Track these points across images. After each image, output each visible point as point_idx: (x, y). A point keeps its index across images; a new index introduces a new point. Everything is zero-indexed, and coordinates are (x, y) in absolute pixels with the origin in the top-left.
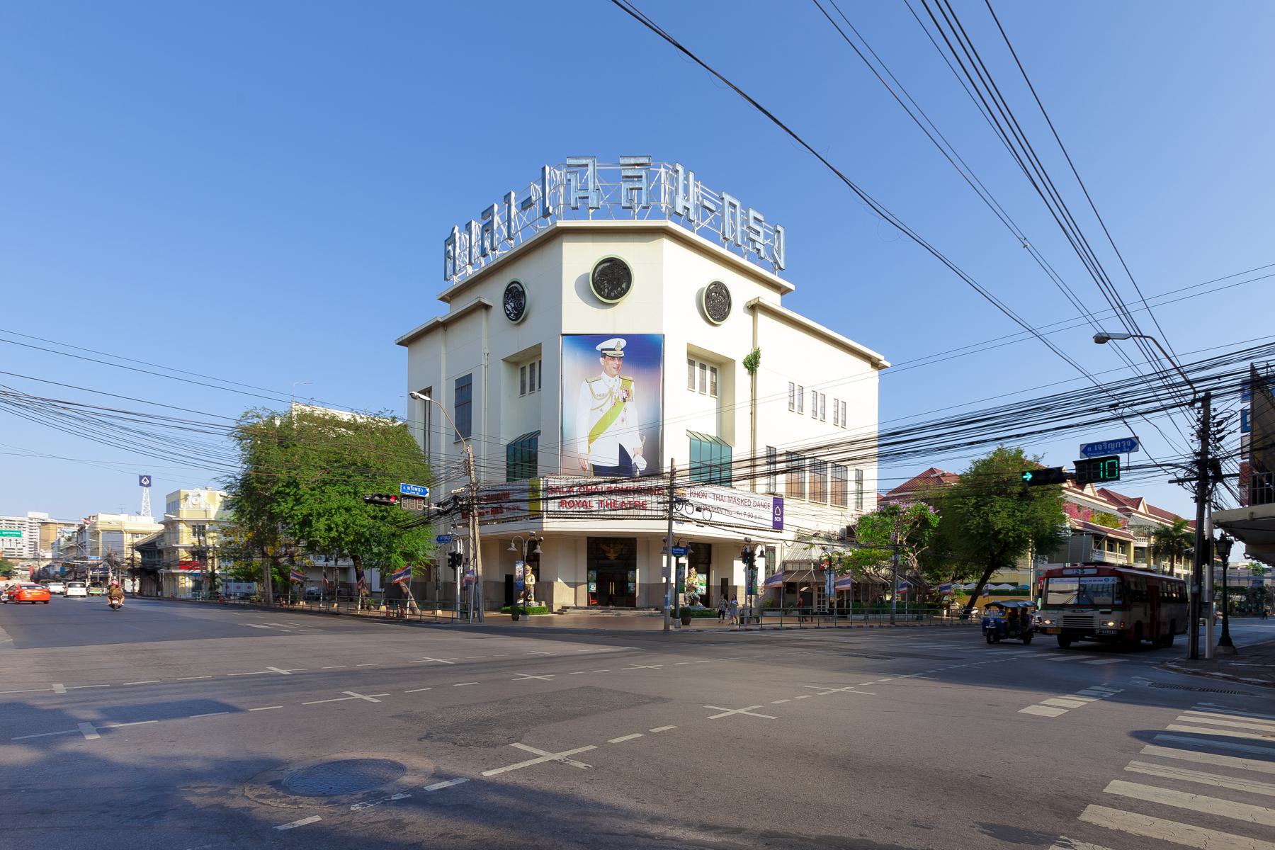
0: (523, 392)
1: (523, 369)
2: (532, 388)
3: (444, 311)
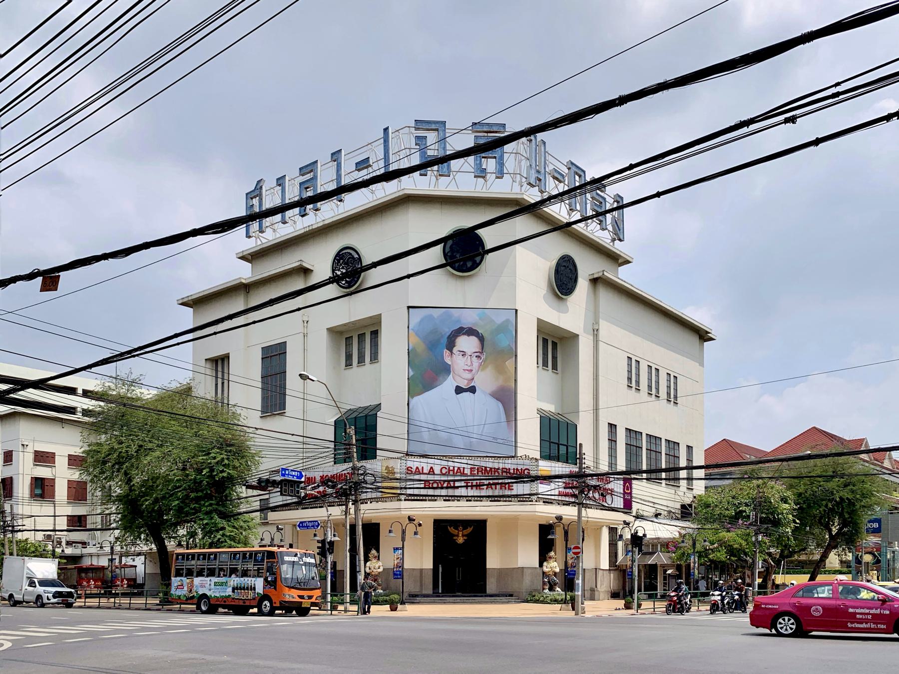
0: (349, 364)
1: (349, 340)
2: (361, 360)
3: (245, 272)
